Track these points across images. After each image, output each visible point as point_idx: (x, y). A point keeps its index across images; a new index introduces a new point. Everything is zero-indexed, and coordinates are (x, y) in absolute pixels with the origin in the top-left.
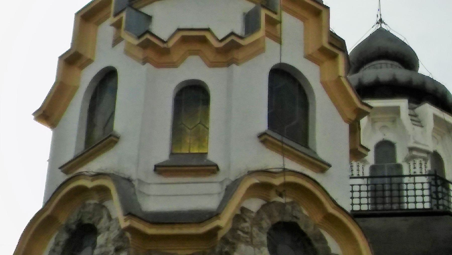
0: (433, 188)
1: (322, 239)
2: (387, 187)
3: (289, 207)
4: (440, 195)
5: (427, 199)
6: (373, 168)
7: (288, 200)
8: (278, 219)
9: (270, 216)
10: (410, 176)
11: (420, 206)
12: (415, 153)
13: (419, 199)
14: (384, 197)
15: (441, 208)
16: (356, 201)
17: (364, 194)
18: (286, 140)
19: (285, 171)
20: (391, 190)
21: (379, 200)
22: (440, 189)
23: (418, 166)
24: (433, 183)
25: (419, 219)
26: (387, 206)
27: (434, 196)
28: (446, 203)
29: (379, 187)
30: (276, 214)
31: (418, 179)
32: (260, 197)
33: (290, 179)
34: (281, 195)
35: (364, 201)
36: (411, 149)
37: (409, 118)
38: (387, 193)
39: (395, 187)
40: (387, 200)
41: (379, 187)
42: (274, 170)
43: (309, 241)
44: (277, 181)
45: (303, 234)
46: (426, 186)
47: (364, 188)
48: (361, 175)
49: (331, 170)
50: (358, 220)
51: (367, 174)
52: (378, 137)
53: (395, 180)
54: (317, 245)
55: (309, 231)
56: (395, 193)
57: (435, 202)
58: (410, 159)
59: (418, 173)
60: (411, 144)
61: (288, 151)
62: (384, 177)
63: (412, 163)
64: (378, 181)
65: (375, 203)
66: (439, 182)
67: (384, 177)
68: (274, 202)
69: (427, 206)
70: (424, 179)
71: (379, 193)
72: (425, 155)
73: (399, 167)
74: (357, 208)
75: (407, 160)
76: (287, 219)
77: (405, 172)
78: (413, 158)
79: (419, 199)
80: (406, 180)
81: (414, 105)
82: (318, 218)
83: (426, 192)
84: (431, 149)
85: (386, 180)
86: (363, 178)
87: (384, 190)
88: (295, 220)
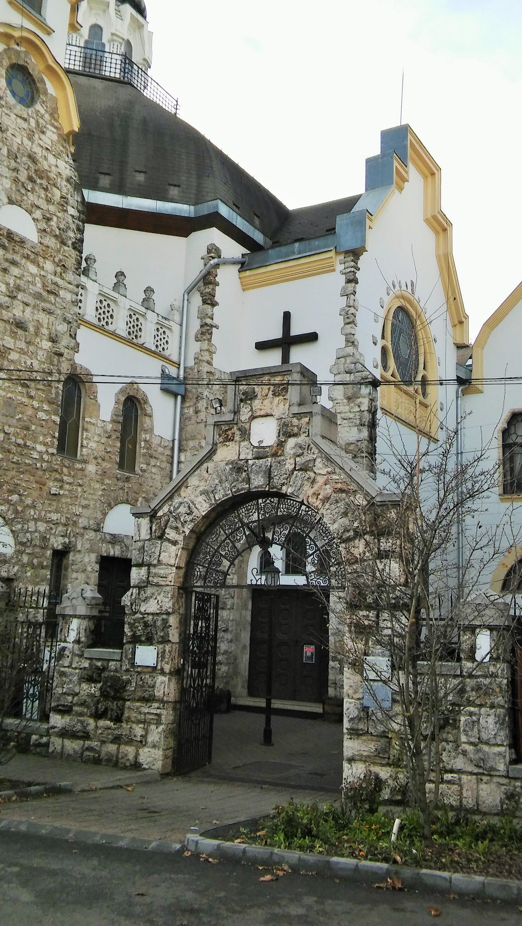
0: (123, 65)
1: (43, 81)
2: (94, 57)
3: (23, 55)
4: (127, 70)
5: (118, 71)
6: (86, 42)
7: (23, 49)
8: (14, 61)
9: (9, 58)
10: (110, 53)
11: (112, 75)
12: (115, 38)
13: (113, 70)
14: (90, 63)
15: (126, 79)
16: (72, 62)
17: (78, 58)
18: (25, 5)
19: (22, 28)
20: (96, 60)
21: (87, 65)
22: (127, 66)
23: (115, 47)
24: (123, 61)
25: (110, 83)
26: (92, 70)
27: (123, 71)
28: (129, 76)
29: (88, 56)
30: (13, 57)
31: (114, 56)
32: (4, 43)
33: (25, 34)
34: (18, 45)
35: (77, 63)
36: (113, 34)
37: (114, 12)
38: (93, 61)
39: (99, 58)
40: (93, 66)
41: (88, 56)
42: (15, 25)
43: (34, 81)
44: (17, 34)
45: (29, 74)
46: (119, 62)
47: (78, 54)
48: (78, 45)
49: (54, 35)
50: (70, 75)
51: (82, 45)
52: (93, 21)
53: (100, 53)
54: (38, 85)
55: (35, 74)
56: (98, 62)
57: (122, 74)
58: (111, 41)
59: (74, 44)
60: (114, 31)
61: (26, 14)
62: (93, 49)
63: (112, 44)
64: (89, 51)
65: (84, 67)
66: (127, 61)
67: (93, 49)
68: (13, 49)
69: (118, 76)
70: (119, 57)
71: (88, 60)
72: (121, 41)
73: (104, 45)
74: (72, 67)
75: (109, 41)
76: (21, 62)
77: (107, 49)
78: (113, 40)
79: (113, 70)
80: (106, 55)
81: (120, 4)
82: (41, 67)
83: (118, 67)
84: (126, 38)
85: (94, 52)
86: (79, 47)
87: (91, 59)
88: (26, 65)
